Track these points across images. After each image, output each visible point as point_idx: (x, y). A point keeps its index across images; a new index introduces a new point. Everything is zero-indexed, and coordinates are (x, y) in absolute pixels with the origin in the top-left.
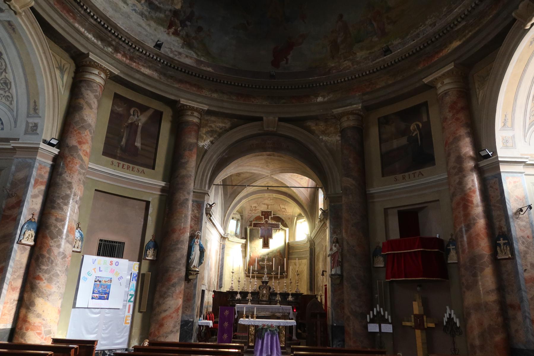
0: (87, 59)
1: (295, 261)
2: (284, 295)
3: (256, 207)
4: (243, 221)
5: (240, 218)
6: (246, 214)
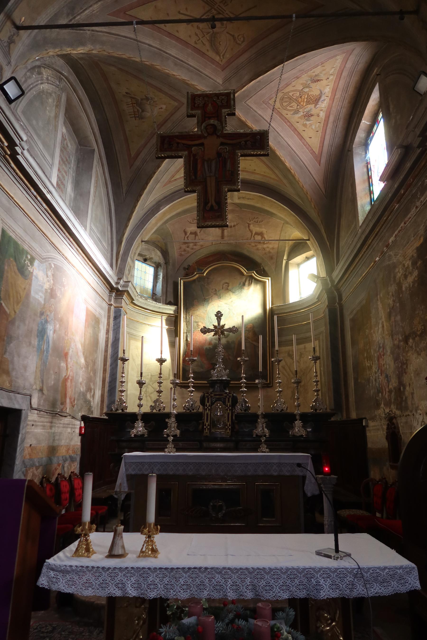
1: (289, 348)
2: (279, 422)
4: (170, 267)
6: (175, 252)
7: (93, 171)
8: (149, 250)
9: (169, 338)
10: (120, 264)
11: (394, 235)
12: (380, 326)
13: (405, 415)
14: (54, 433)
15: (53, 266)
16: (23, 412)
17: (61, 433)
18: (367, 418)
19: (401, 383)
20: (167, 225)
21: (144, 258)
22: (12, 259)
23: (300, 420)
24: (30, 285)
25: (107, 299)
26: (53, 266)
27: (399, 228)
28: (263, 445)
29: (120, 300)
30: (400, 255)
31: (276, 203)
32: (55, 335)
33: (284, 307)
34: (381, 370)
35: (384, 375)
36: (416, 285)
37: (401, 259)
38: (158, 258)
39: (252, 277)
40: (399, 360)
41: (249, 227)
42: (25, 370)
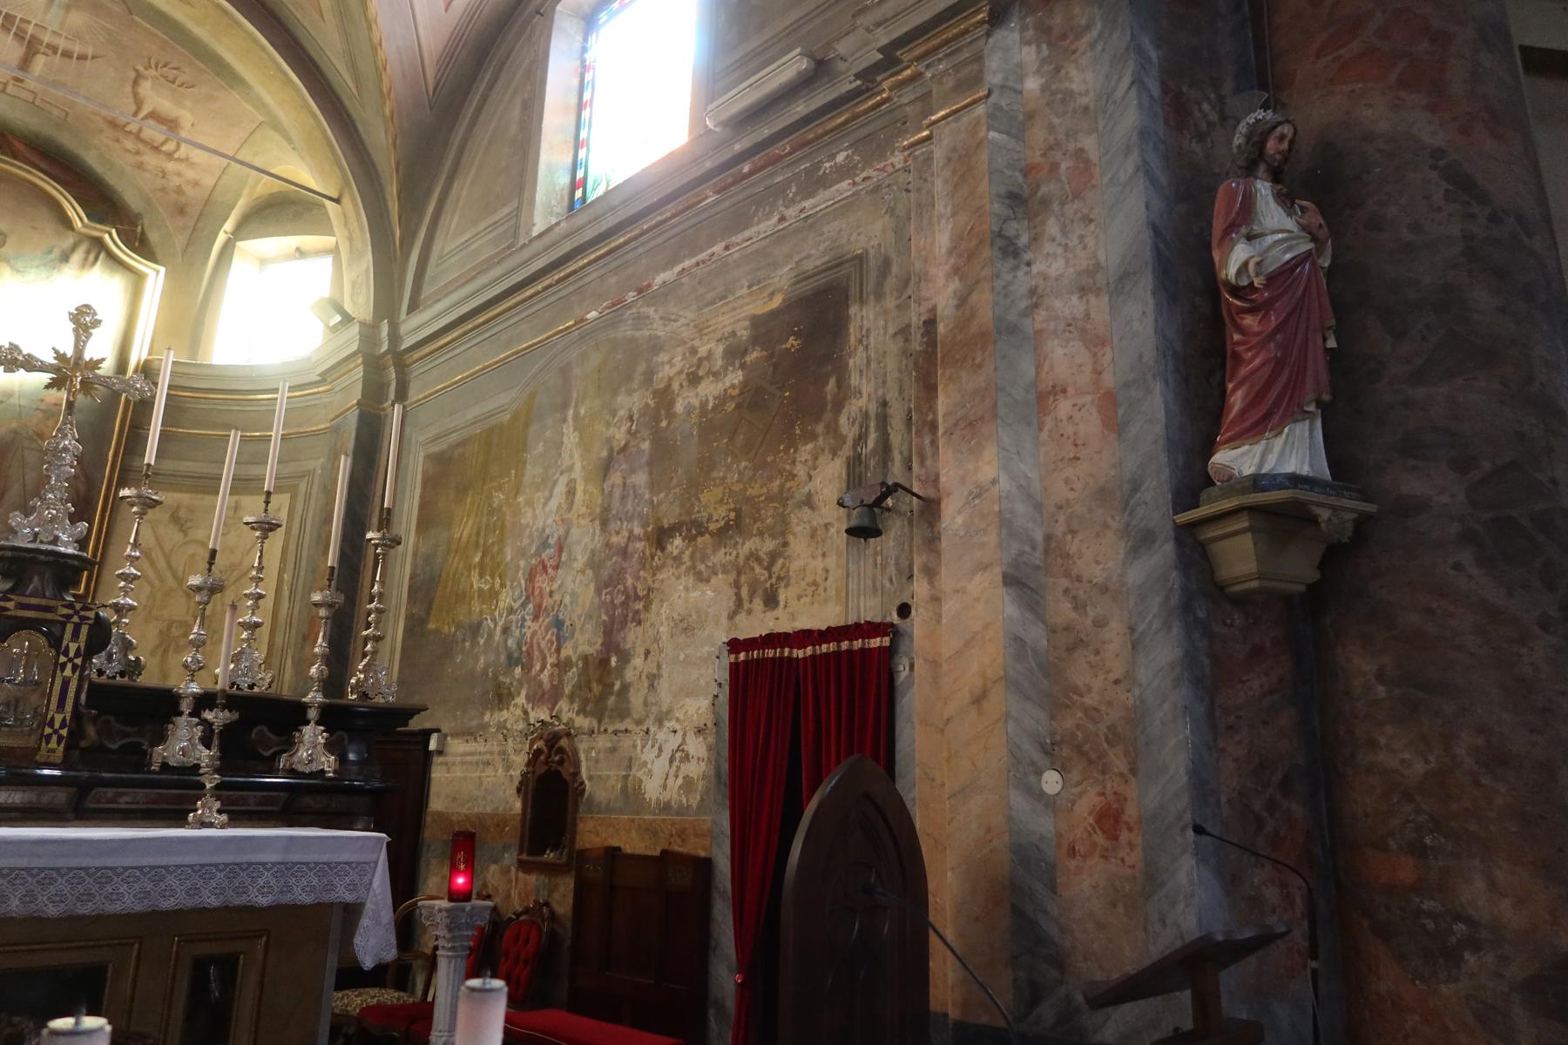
11: (679, 268)
12: (561, 488)
13: (610, 729)
18: (445, 730)
19: (611, 644)
23: (318, 723)
27: (703, 256)
28: (208, 799)
30: (683, 321)
31: (269, 54)
33: (192, 371)
34: (539, 607)
35: (545, 620)
36: (730, 406)
37: (686, 334)
39: (98, 245)
40: (621, 587)
41: (136, 83)
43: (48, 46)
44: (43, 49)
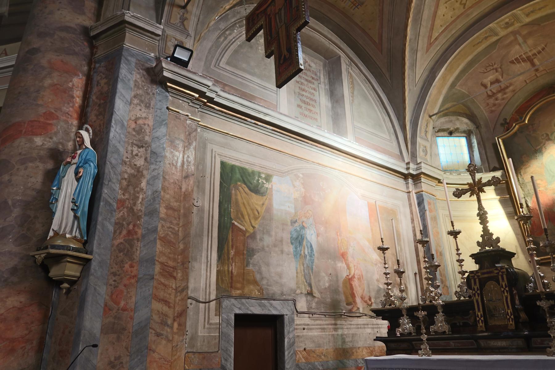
0: (263, 188)
3: (497, 81)
4: (483, 130)
5: (471, 126)
6: (483, 111)
7: (343, 75)
8: (451, 121)
9: (504, 210)
10: (411, 148)
14: (342, 335)
15: (301, 176)
16: (286, 318)
17: (353, 335)
20: (457, 87)
21: (448, 131)
22: (239, 183)
24: (271, 199)
25: (404, 188)
26: (301, 176)
29: (419, 184)
32: (319, 238)
38: (465, 126)
42: (280, 277)
43: (533, 55)
44: (532, 57)
